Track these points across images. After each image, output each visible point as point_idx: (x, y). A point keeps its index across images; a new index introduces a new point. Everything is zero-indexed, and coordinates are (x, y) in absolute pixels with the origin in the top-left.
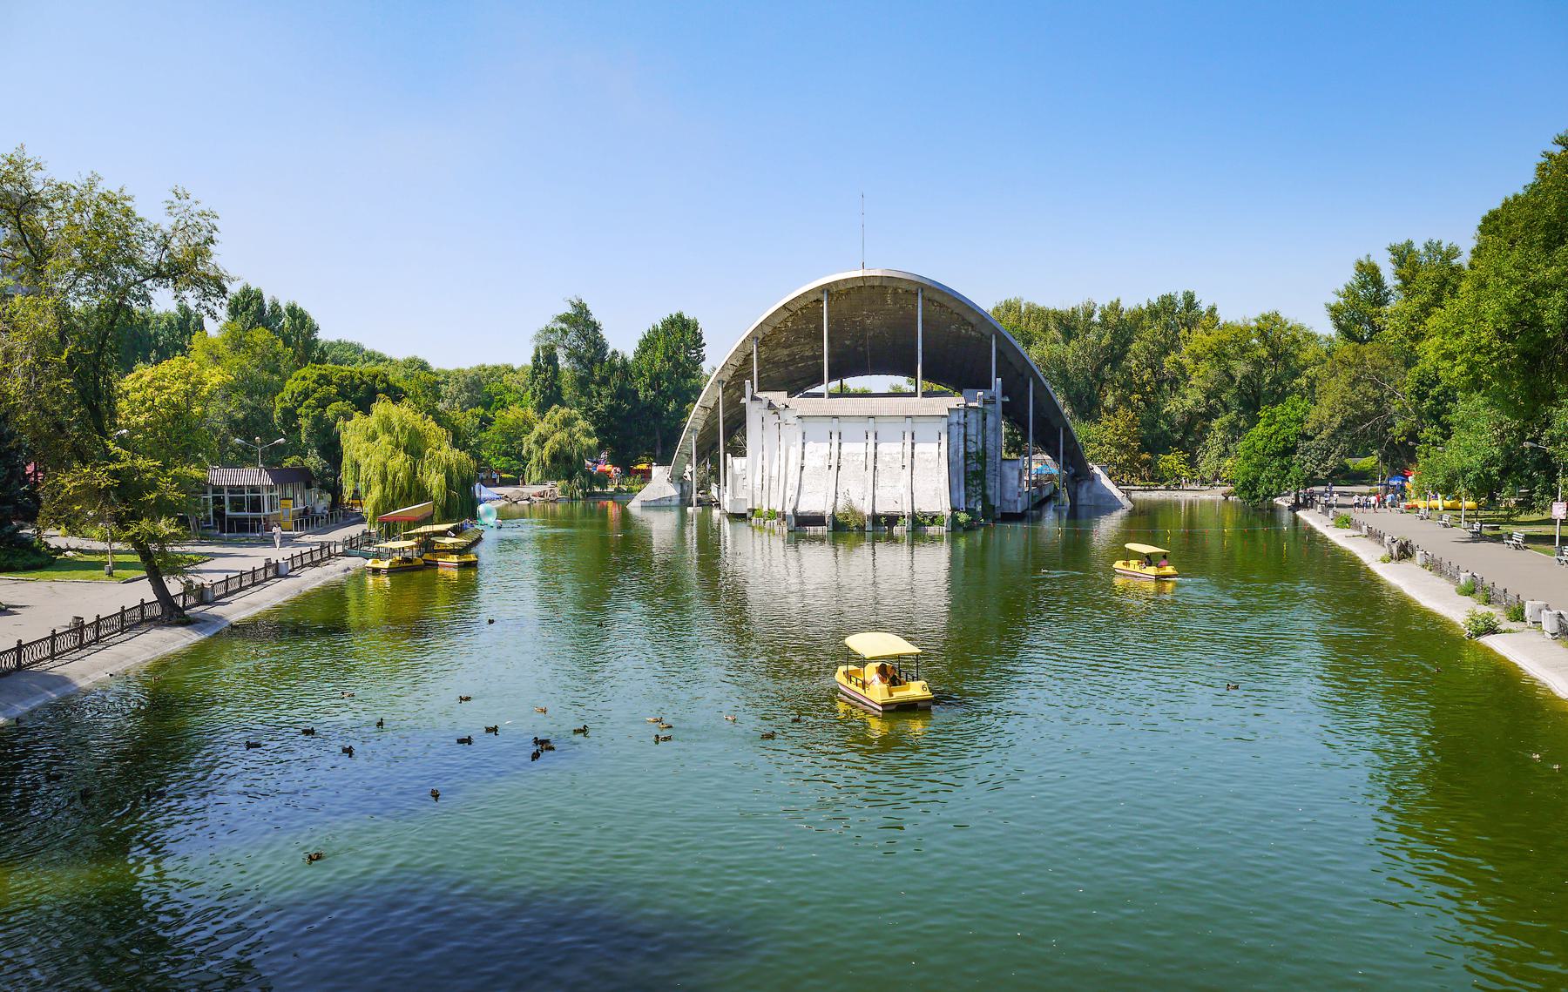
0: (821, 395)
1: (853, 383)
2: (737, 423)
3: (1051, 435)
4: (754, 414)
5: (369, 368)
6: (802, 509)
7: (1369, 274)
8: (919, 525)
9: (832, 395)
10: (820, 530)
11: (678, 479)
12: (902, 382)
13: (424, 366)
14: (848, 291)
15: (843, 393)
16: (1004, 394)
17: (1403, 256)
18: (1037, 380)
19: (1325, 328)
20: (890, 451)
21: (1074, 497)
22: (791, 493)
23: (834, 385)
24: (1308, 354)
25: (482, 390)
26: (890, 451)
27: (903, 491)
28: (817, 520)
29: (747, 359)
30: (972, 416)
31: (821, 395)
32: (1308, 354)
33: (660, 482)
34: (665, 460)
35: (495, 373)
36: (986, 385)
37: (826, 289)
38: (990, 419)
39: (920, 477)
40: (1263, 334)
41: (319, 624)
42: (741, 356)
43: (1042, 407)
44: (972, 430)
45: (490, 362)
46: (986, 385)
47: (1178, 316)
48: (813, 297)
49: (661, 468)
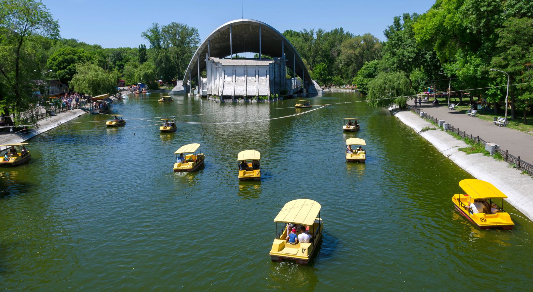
0: (230, 59)
1: (241, 55)
2: (204, 67)
3: (301, 71)
4: (209, 64)
5: (67, 48)
6: (224, 94)
7: (397, 21)
8: (260, 100)
9: (233, 59)
10: (230, 101)
11: (185, 85)
12: (252, 55)
13: (99, 47)
14: (238, 26)
15: (237, 58)
16: (286, 59)
17: (406, 17)
18: (298, 57)
19: (384, 39)
20: (243, 81)
21: (307, 91)
22: (221, 89)
23: (234, 55)
24: (376, 46)
25: (119, 58)
26: (243, 81)
27: (256, 88)
28: (229, 97)
29: (207, 47)
30: (276, 65)
31: (230, 59)
32: (376, 46)
33: (179, 86)
34: (181, 79)
35: (125, 50)
36: (281, 56)
37: (230, 25)
38: (282, 66)
39: (261, 86)
40: (365, 41)
41: (65, 136)
42: (205, 46)
43: (296, 65)
44: (276, 70)
45: (123, 46)
46: (281, 56)
47: (338, 36)
48: (227, 28)
49: (180, 81)
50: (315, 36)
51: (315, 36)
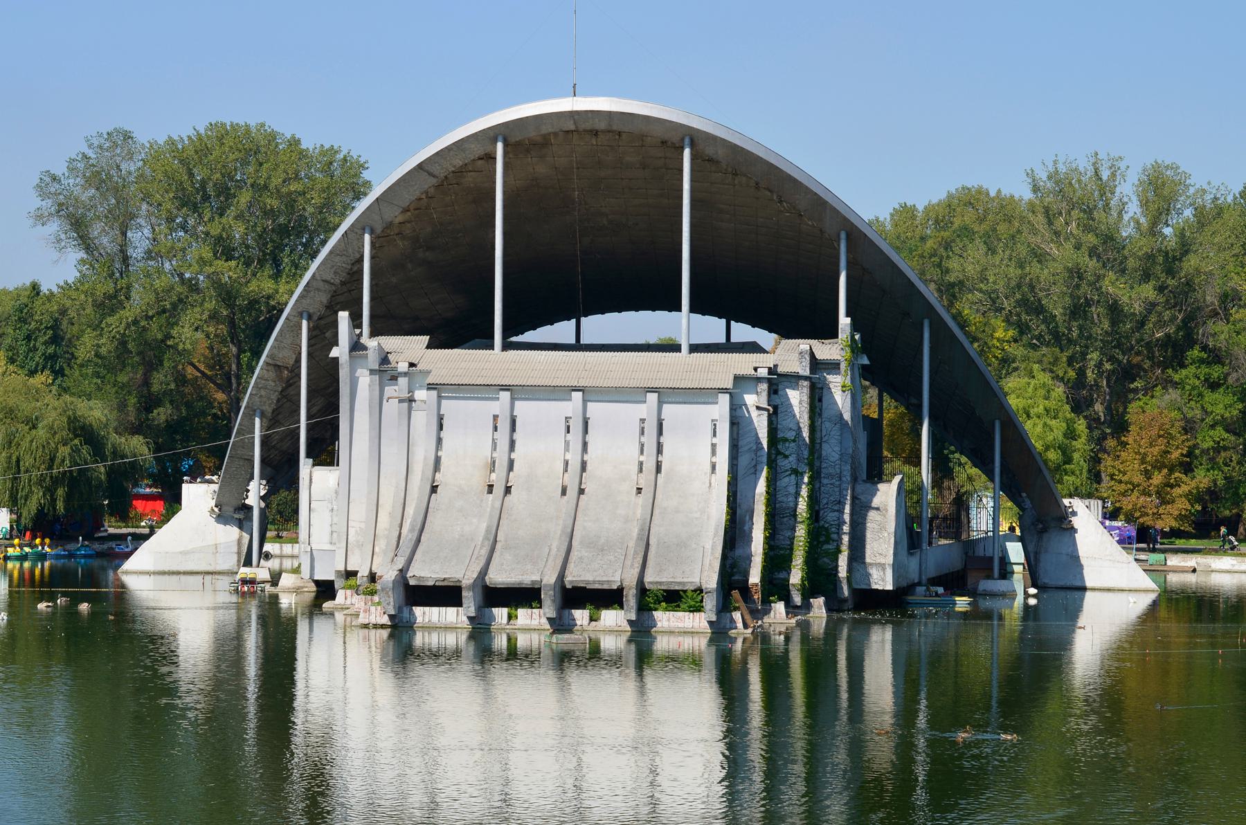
4: (360, 391)
50: (1128, 192)
51: (1128, 192)
